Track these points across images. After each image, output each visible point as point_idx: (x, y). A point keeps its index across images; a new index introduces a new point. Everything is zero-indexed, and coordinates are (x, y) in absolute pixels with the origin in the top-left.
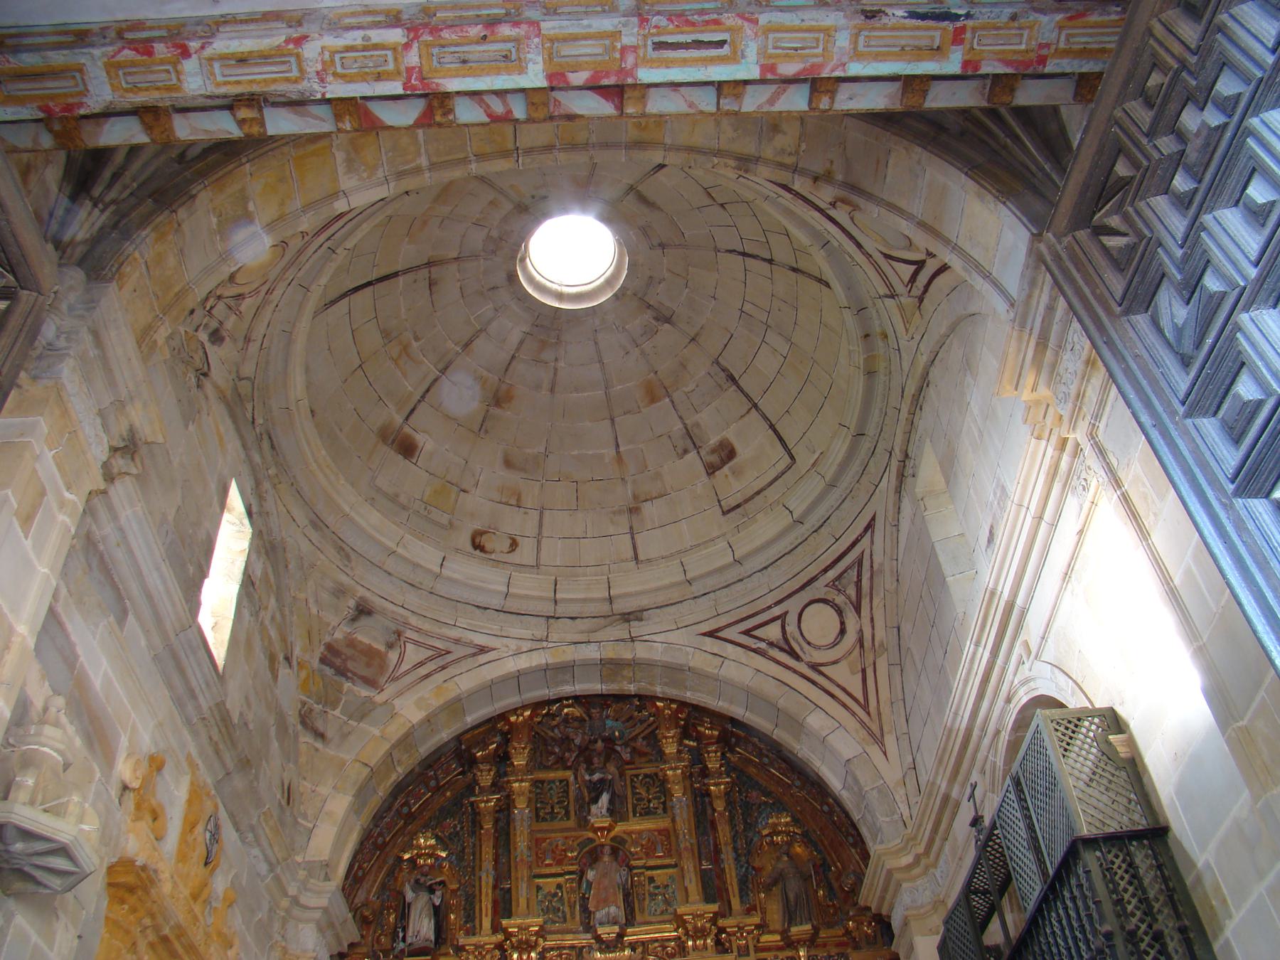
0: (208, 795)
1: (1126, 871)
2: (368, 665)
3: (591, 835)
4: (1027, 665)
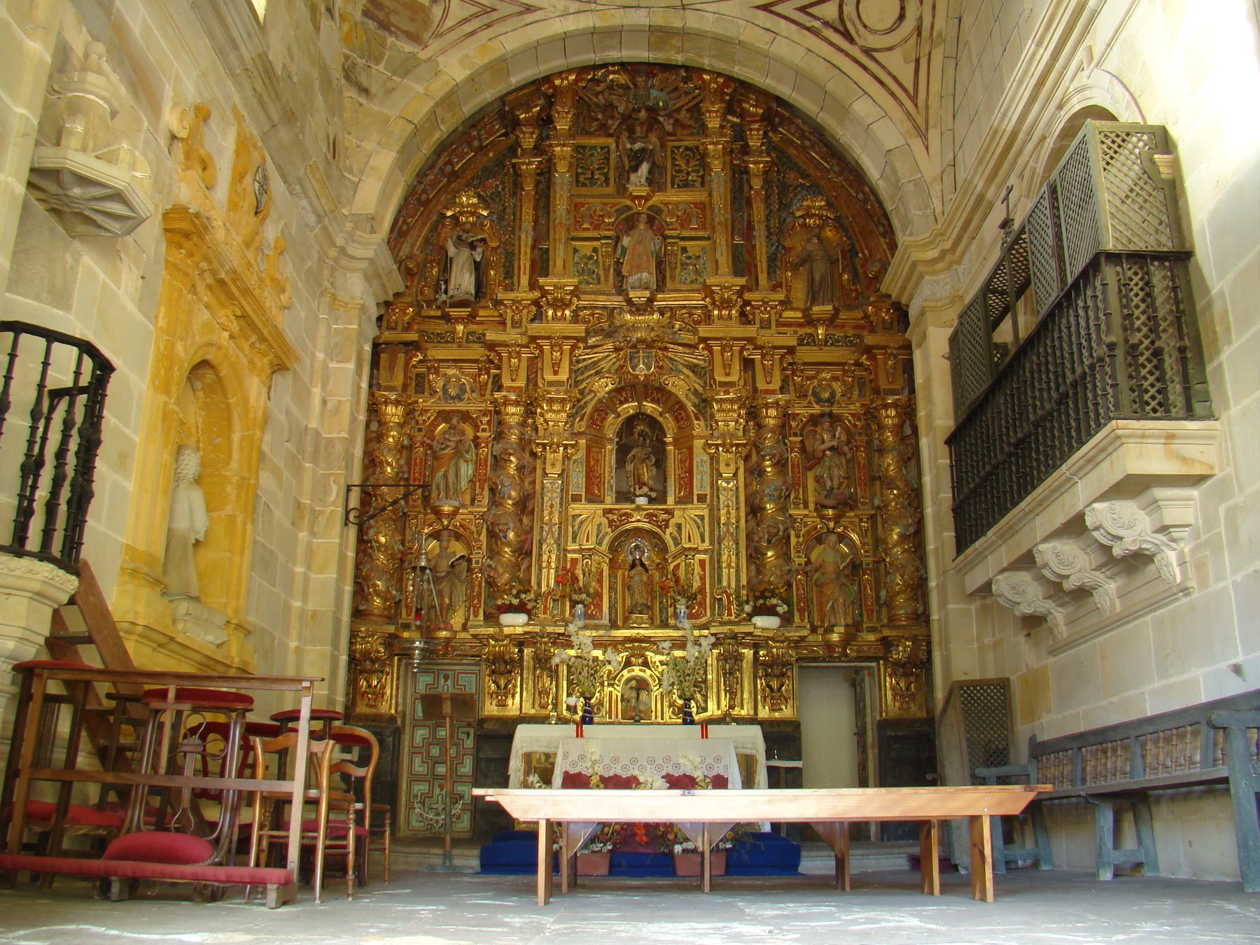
0: (255, 146)
1: (1142, 289)
2: (412, 20)
3: (629, 203)
4: (1086, 72)
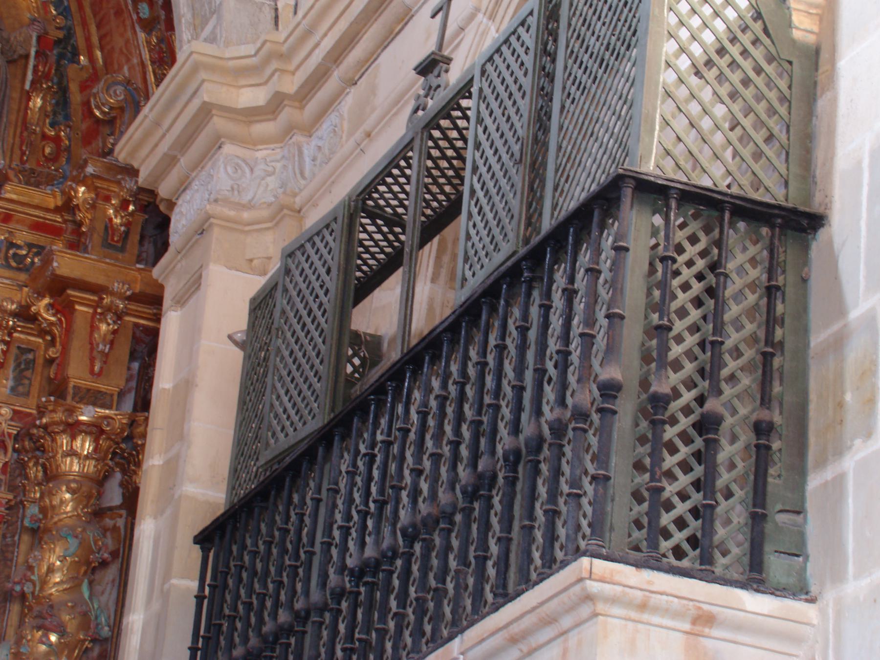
1: (700, 277)
